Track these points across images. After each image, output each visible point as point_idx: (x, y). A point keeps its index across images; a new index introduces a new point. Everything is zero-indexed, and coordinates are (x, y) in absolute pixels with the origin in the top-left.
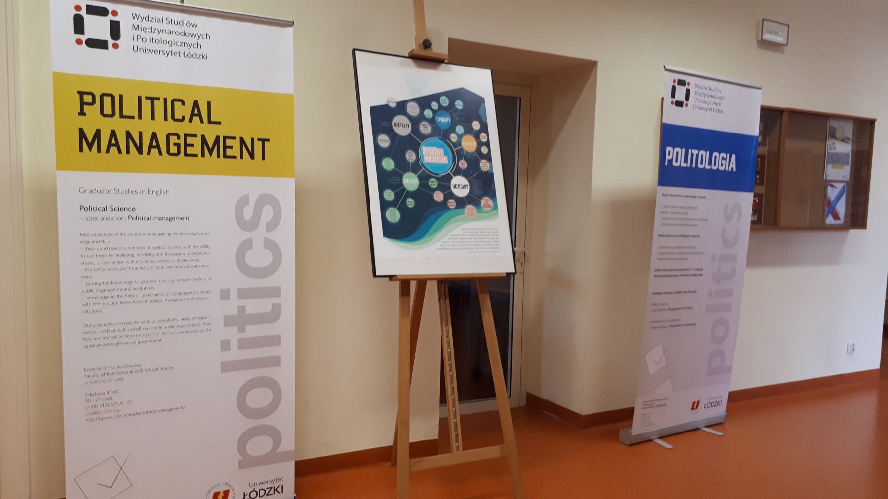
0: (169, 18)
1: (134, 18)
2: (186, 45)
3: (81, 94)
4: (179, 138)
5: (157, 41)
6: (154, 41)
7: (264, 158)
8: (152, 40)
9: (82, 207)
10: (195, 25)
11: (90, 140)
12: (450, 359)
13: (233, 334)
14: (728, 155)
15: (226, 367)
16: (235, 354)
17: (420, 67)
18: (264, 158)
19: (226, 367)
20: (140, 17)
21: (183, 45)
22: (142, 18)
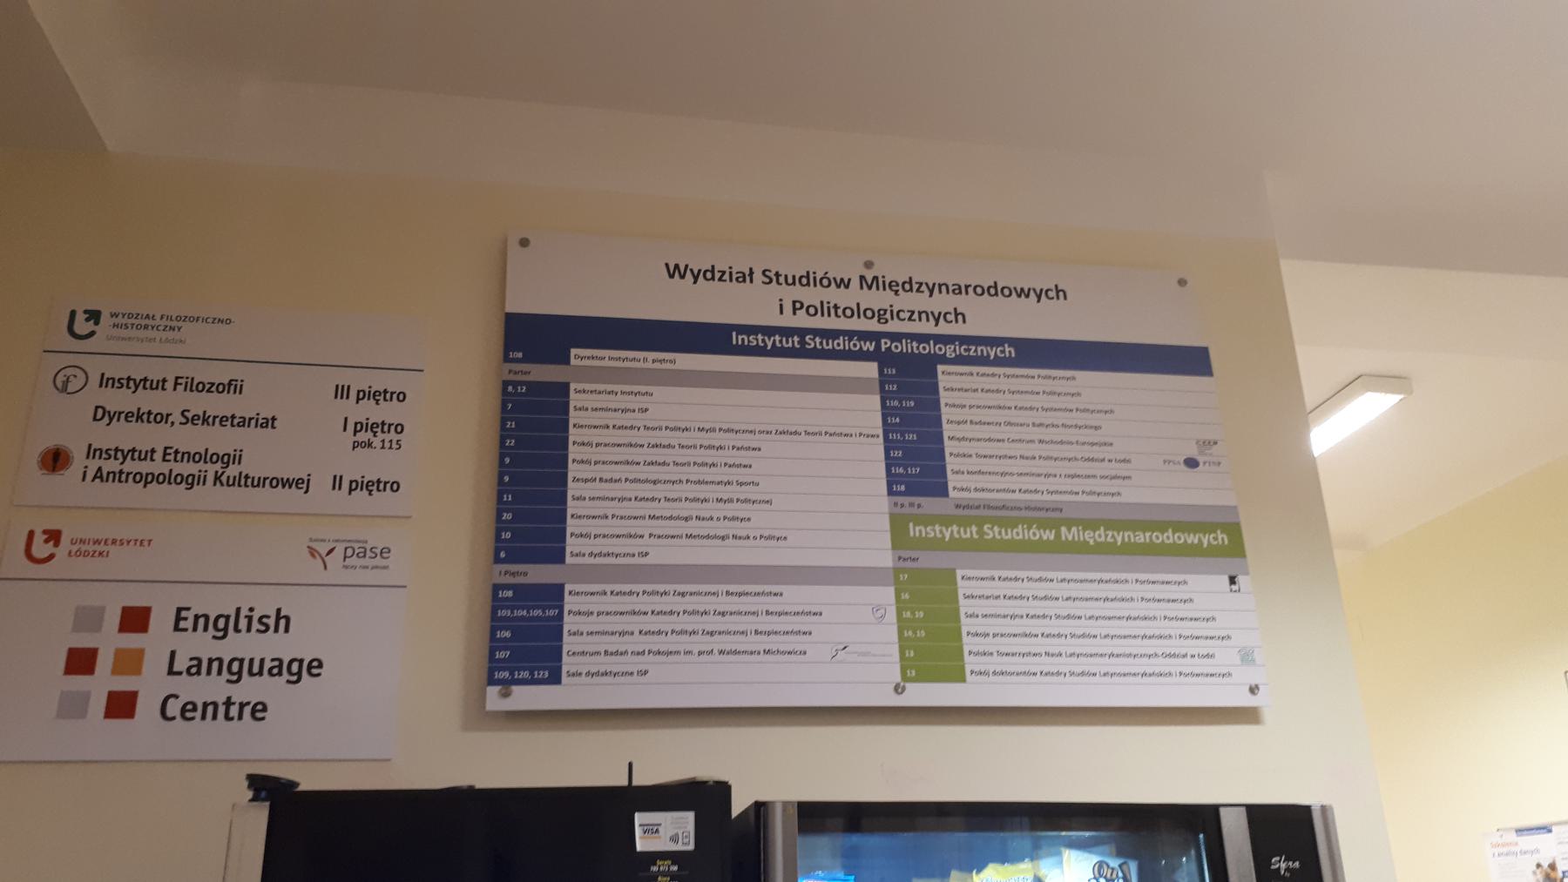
0: (376, 548)
1: (672, 276)
2: (924, 316)
3: (794, 302)
4: (898, 285)
5: (848, 312)
6: (840, 312)
7: (346, 419)
8: (832, 311)
9: (798, 305)
10: (526, 574)
11: (870, 283)
12: (611, 359)
13: (832, 305)
14: (1132, 540)
15: (822, 303)
16: (826, 306)
17: (694, 778)
18: (346, 419)
19: (822, 303)
20: (688, 272)
21: (916, 316)
22: (696, 272)
